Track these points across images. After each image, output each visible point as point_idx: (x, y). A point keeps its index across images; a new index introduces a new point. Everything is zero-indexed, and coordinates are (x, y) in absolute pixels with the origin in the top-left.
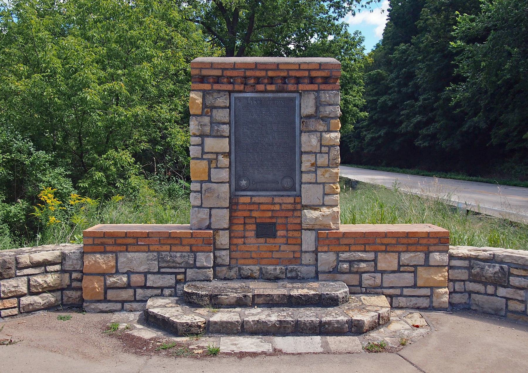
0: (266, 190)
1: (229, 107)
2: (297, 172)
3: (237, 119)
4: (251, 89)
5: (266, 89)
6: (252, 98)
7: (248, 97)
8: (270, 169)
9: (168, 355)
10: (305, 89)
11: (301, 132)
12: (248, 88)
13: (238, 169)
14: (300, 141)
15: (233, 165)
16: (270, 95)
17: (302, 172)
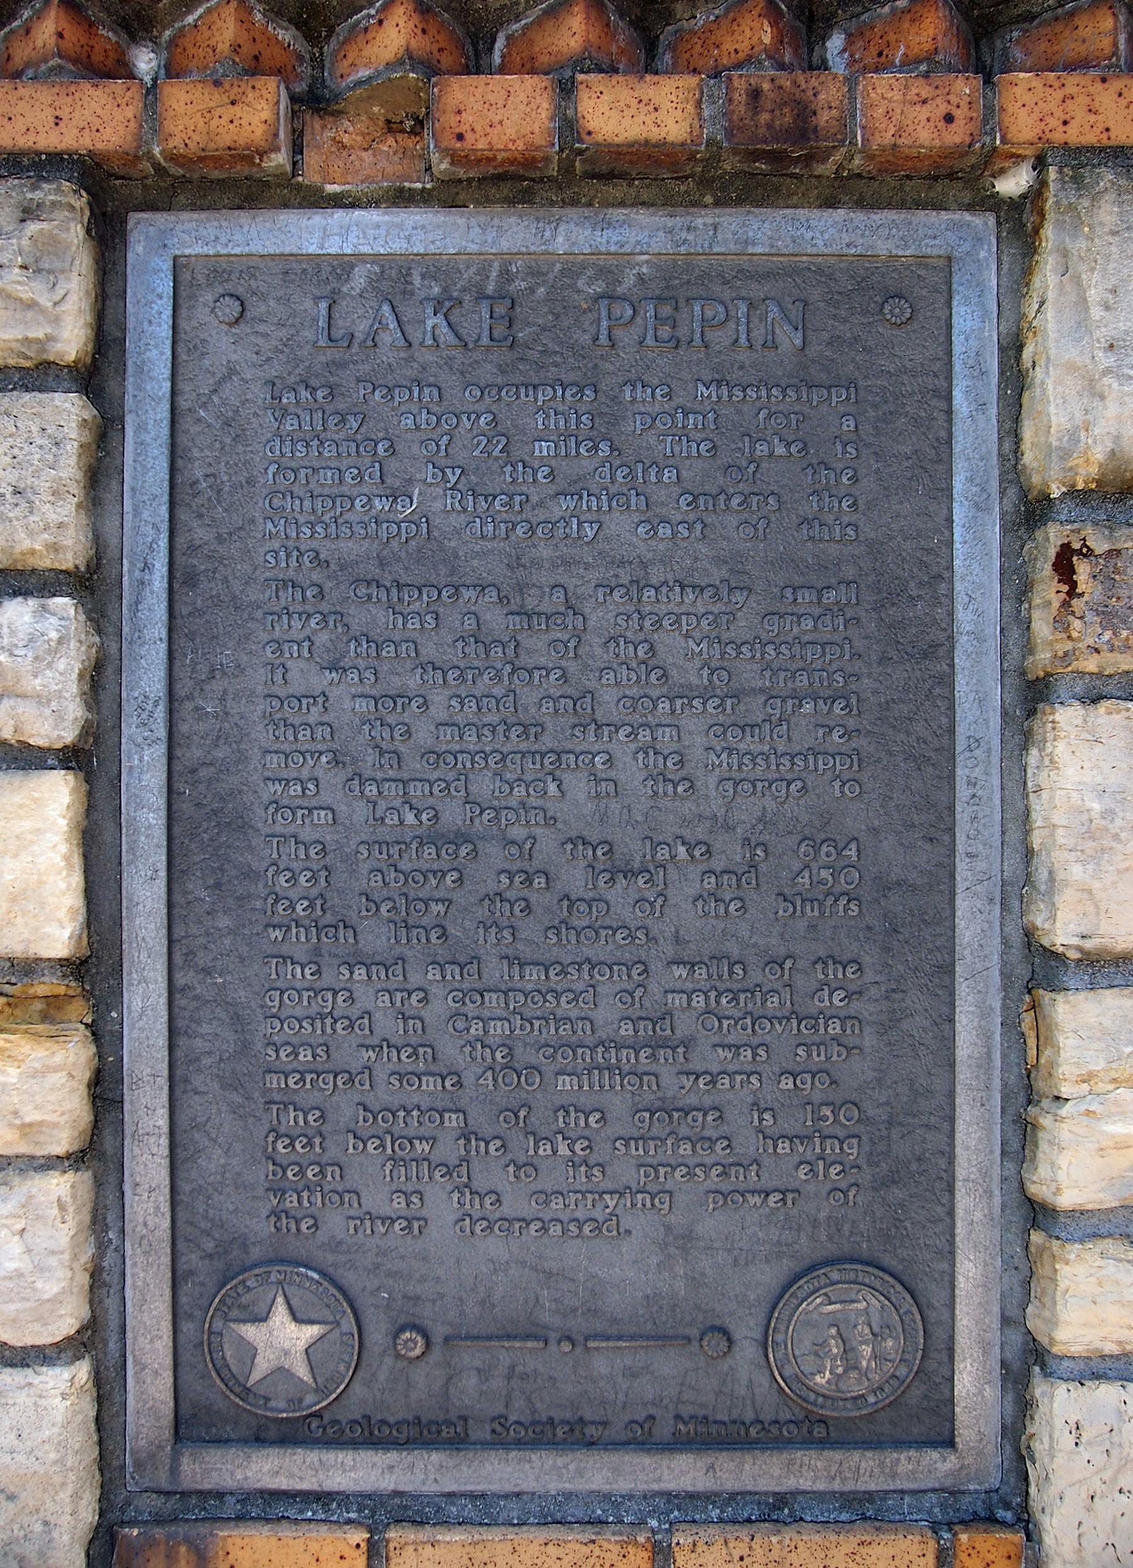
0: (574, 1434)
1: (97, 375)
2: (974, 1210)
3: (201, 533)
4: (383, 162)
5: (569, 127)
6: (394, 277)
7: (344, 265)
8: (625, 1172)
9: (861, 204)
10: (1081, 132)
11: (1032, 695)
12: (348, 151)
13: (211, 1162)
14: (1019, 817)
15: (147, 1109)
16: (640, 234)
17: (1037, 1214)
